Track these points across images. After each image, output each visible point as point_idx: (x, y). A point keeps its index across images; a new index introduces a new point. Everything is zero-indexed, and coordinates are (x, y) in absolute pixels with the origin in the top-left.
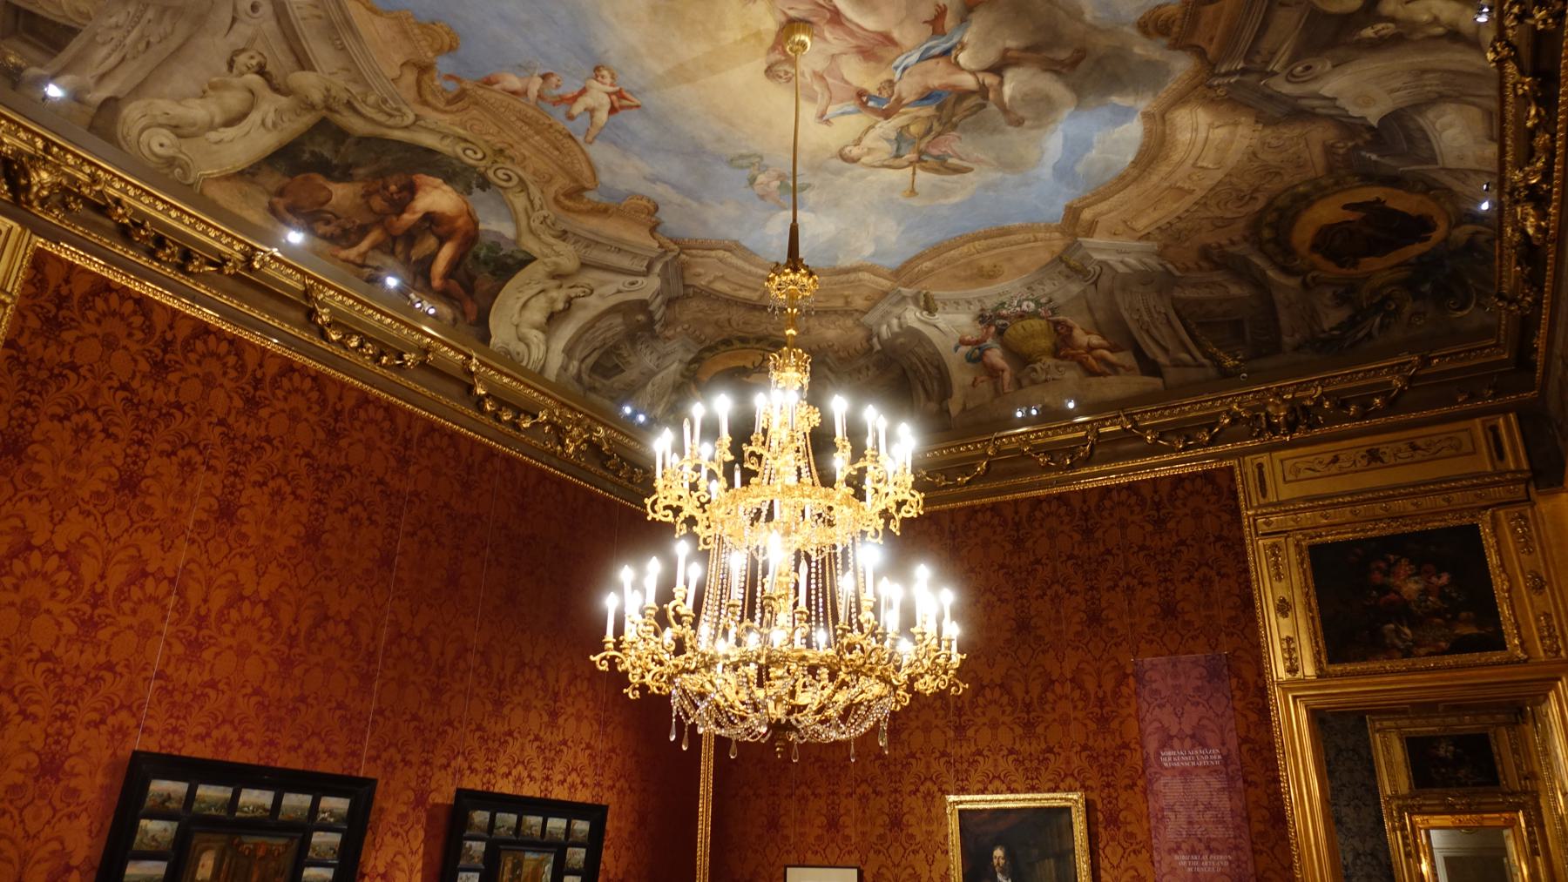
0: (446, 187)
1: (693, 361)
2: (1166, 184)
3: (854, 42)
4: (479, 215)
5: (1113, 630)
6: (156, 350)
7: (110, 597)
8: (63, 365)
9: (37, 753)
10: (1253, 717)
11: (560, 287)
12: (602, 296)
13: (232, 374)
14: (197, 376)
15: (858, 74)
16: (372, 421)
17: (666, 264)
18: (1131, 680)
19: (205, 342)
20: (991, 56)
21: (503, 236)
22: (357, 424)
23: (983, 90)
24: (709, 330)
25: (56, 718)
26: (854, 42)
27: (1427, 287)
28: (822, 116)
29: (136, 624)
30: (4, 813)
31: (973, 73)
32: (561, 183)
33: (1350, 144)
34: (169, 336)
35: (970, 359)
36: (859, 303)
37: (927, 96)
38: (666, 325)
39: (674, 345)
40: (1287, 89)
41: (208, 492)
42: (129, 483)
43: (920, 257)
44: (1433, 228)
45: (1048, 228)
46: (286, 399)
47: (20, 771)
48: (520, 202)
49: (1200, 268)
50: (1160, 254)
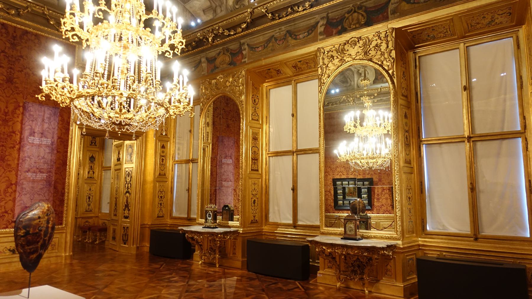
5: (17, 87)
8: (11, 132)
10: (64, 131)
18: (21, 109)
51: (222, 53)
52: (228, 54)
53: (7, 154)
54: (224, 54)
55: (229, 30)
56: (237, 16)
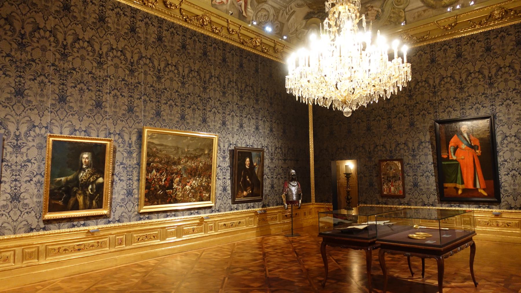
6: (18, 38)
7: (23, 136)
8: (29, 60)
9: (9, 193)
13: (54, 44)
14: (112, 65)
16: (194, 77)
19: (39, 33)
22: (190, 79)
25: (13, 181)
29: (35, 145)
30: (3, 215)
34: (65, 43)
41: (53, 92)
42: (131, 110)
46: (78, 52)
47: (4, 200)
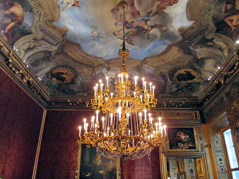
0: (21, 8)
1: (54, 68)
2: (162, 59)
3: (132, 11)
4: (25, 18)
8: (72, 162)
11: (34, 42)
12: (42, 47)
15: (128, 18)
17: (61, 45)
20: (153, 24)
21: (28, 25)
23: (147, 30)
24: (61, 62)
26: (132, 11)
27: (189, 88)
28: (115, 24)
31: (148, 26)
32: (50, 17)
33: (193, 61)
35: (111, 82)
36: (96, 65)
37: (137, 27)
38: (52, 59)
39: (51, 63)
40: (192, 49)
43: (113, 59)
44: (194, 78)
45: (139, 61)
48: (37, 18)
49: (158, 76)
50: (154, 71)
51: (232, 87)
52: (236, 86)
53: (131, 174)
54: (233, 87)
55: (230, 71)
56: (231, 60)
